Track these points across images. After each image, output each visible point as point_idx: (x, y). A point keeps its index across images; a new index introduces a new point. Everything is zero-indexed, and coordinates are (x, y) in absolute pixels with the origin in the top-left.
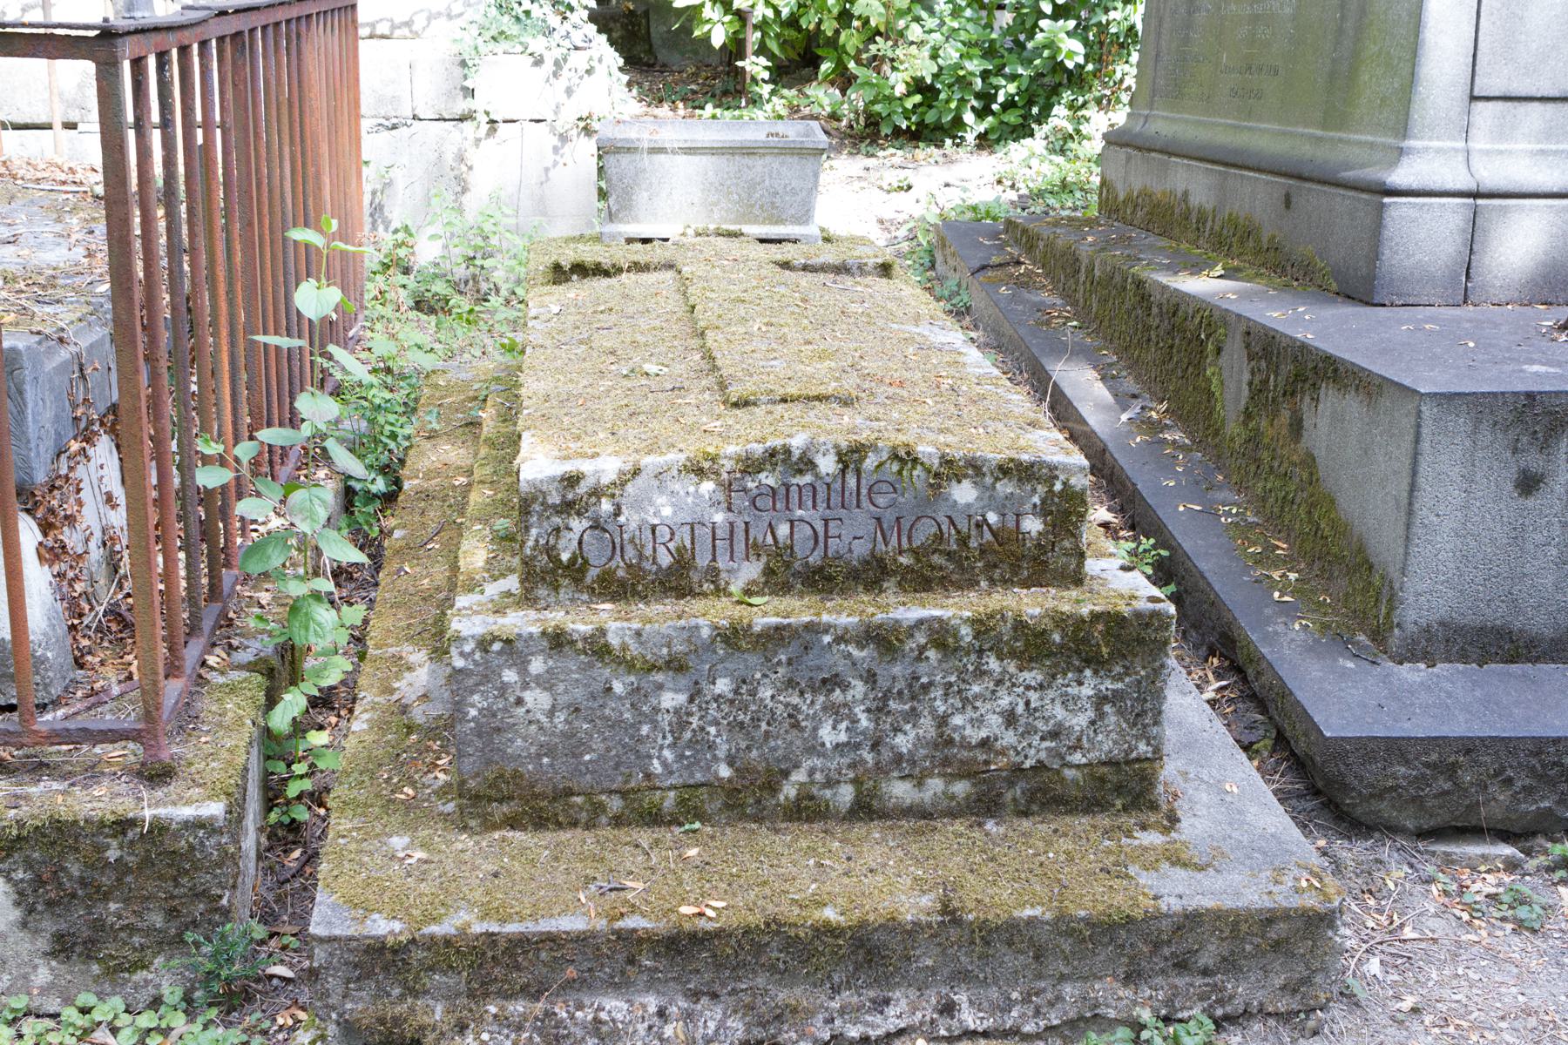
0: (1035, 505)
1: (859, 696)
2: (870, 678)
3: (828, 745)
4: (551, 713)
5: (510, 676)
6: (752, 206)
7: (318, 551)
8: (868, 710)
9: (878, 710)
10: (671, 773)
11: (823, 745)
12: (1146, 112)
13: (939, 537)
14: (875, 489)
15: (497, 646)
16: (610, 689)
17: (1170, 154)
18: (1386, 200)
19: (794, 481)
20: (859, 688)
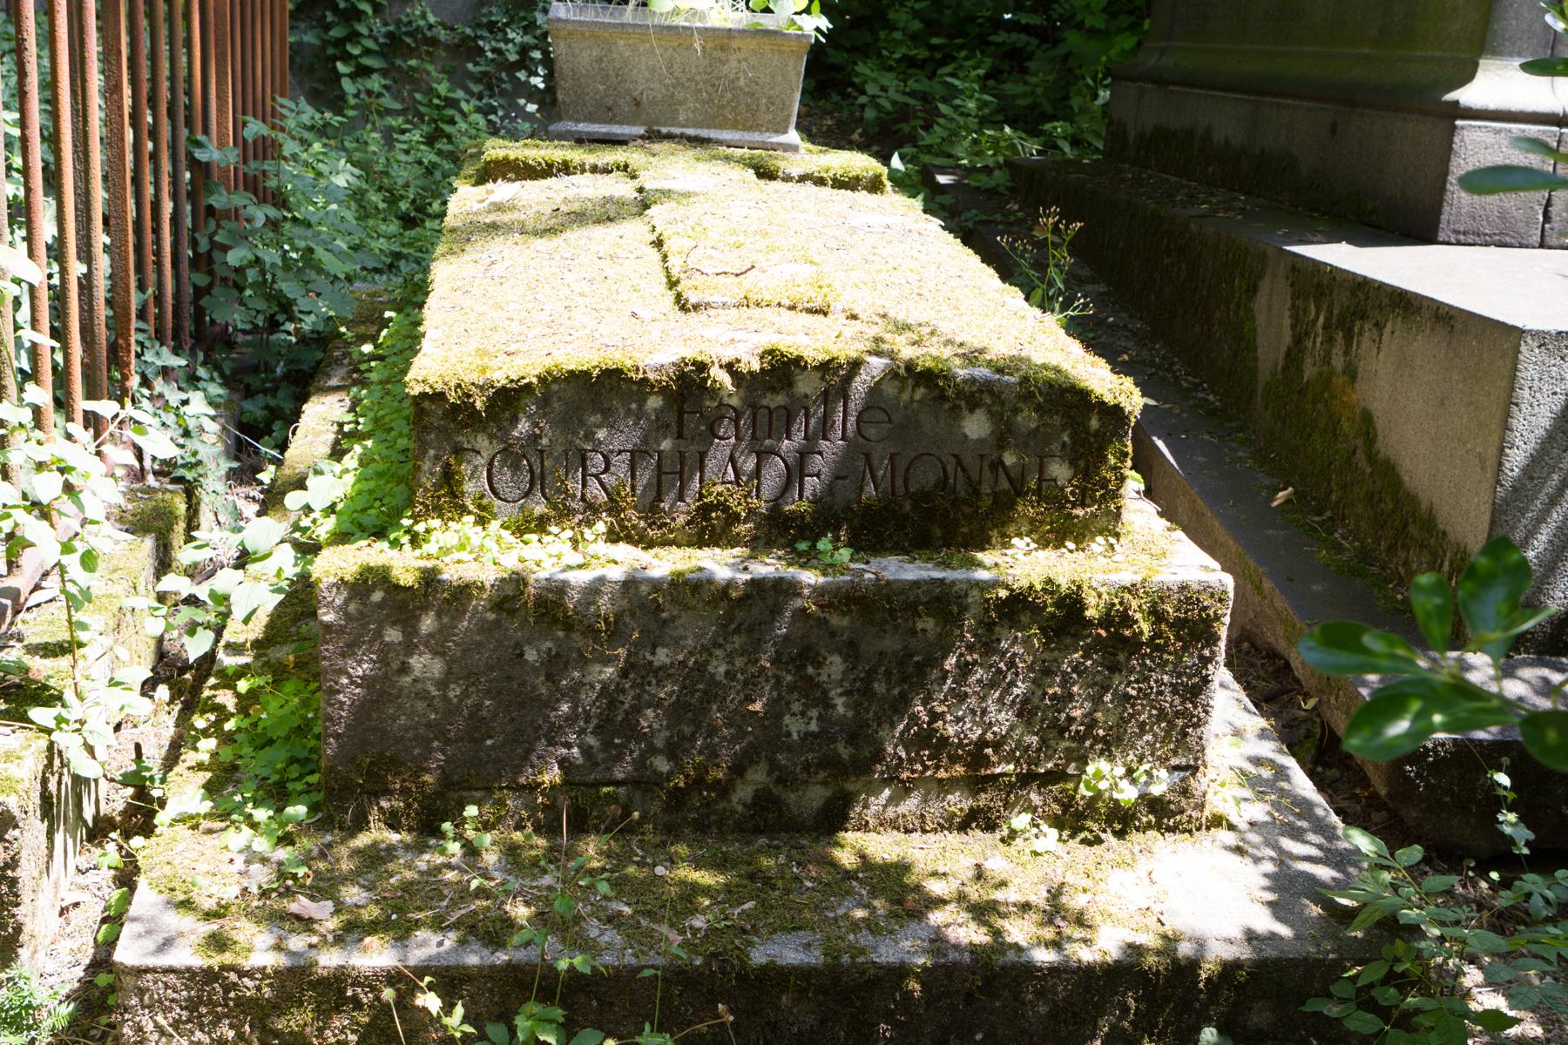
0: (1064, 445)
1: (837, 676)
2: (851, 651)
3: (795, 736)
4: (443, 684)
5: (393, 635)
6: (723, 107)
7: (872, 932)
8: (847, 693)
9: (861, 692)
10: (596, 764)
11: (789, 734)
12: (1163, 44)
13: (943, 483)
14: (865, 417)
15: (377, 596)
16: (522, 655)
17: (1192, 86)
18: (1459, 123)
19: (765, 402)
20: (835, 665)
